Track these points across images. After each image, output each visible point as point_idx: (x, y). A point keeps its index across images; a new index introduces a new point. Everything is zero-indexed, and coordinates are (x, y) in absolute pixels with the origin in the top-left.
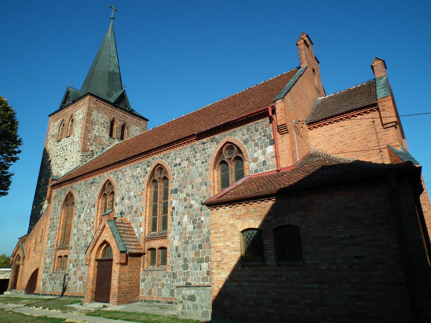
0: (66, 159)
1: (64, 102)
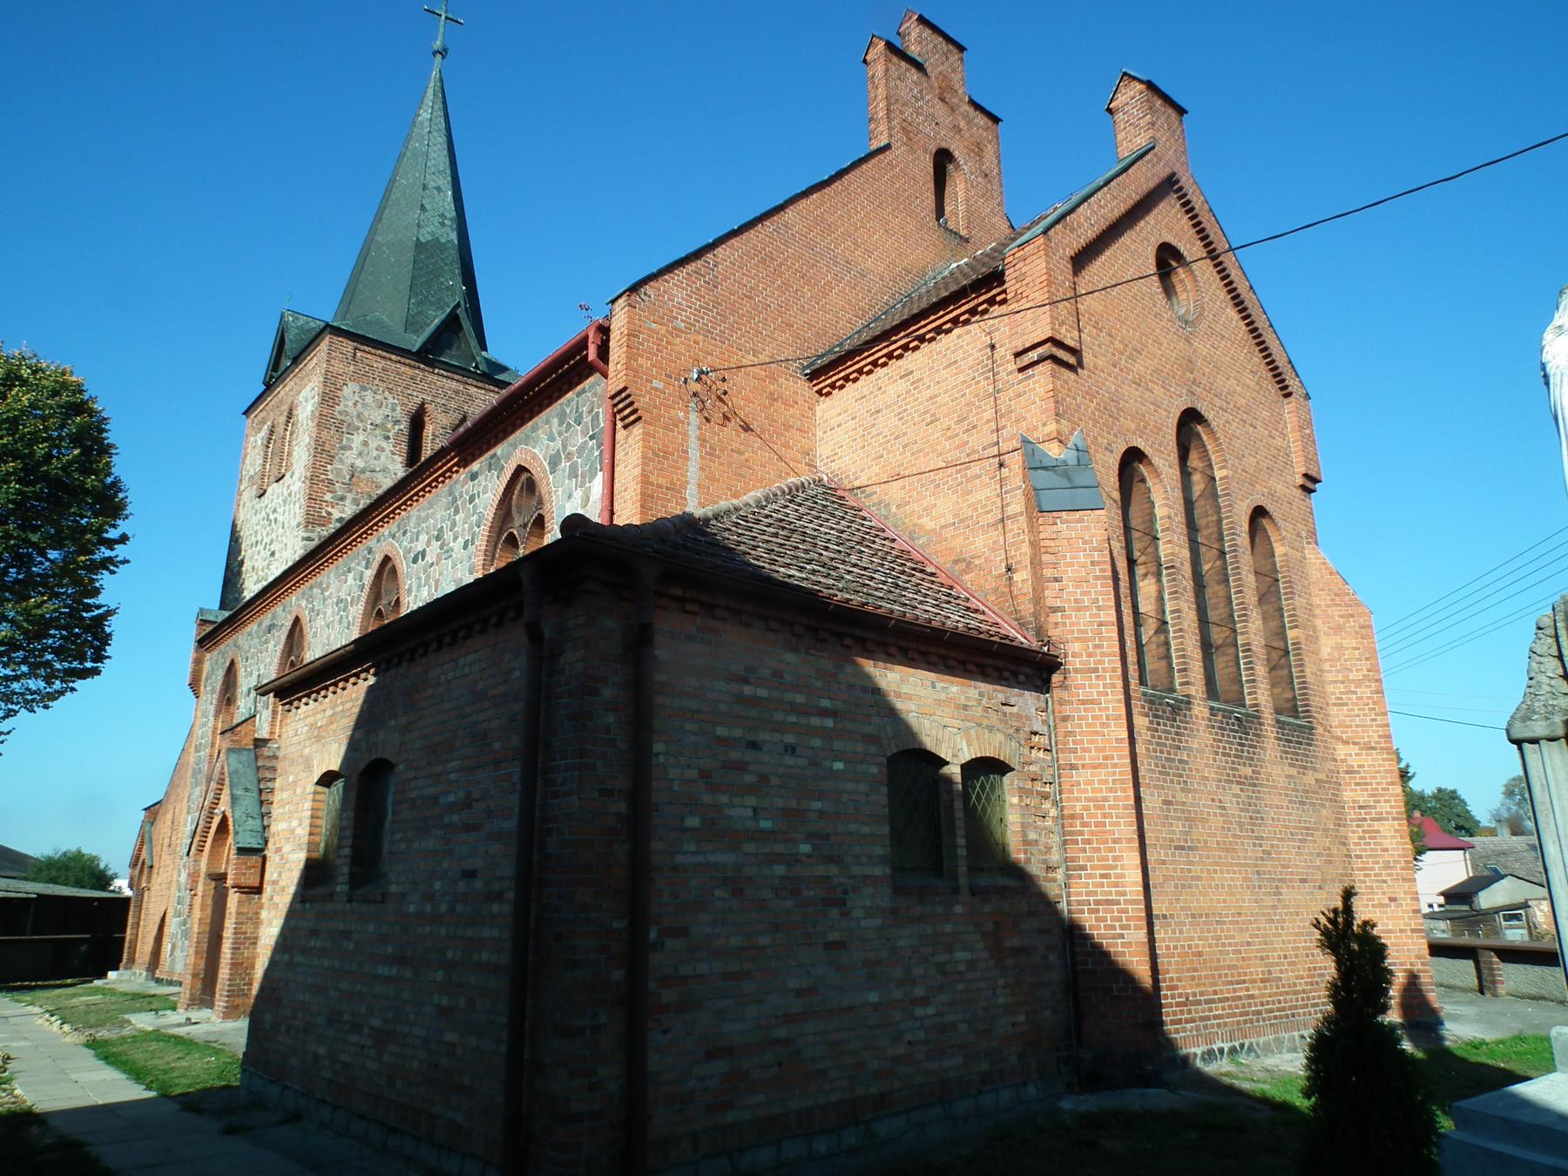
1: (275, 364)
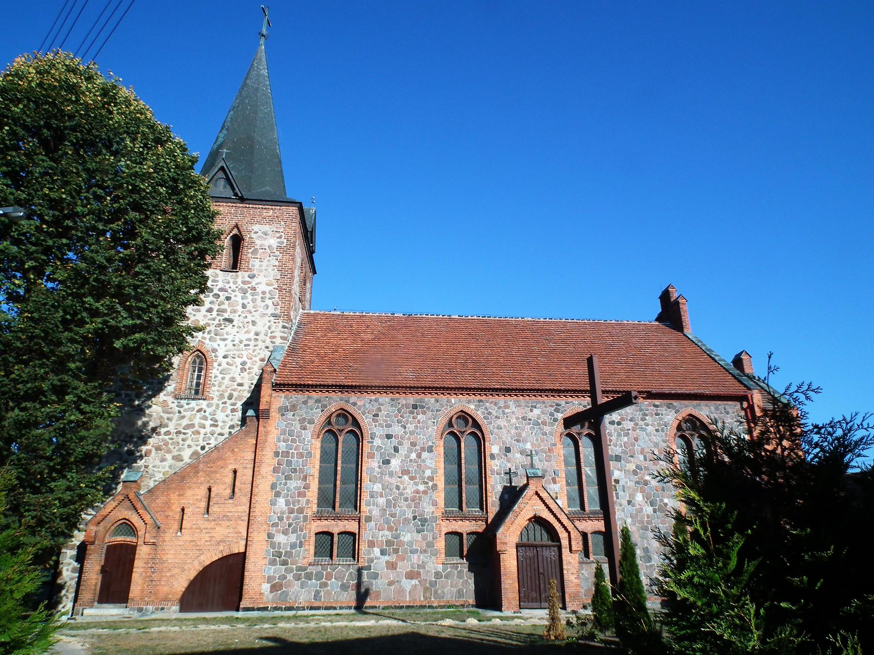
0: (230, 321)
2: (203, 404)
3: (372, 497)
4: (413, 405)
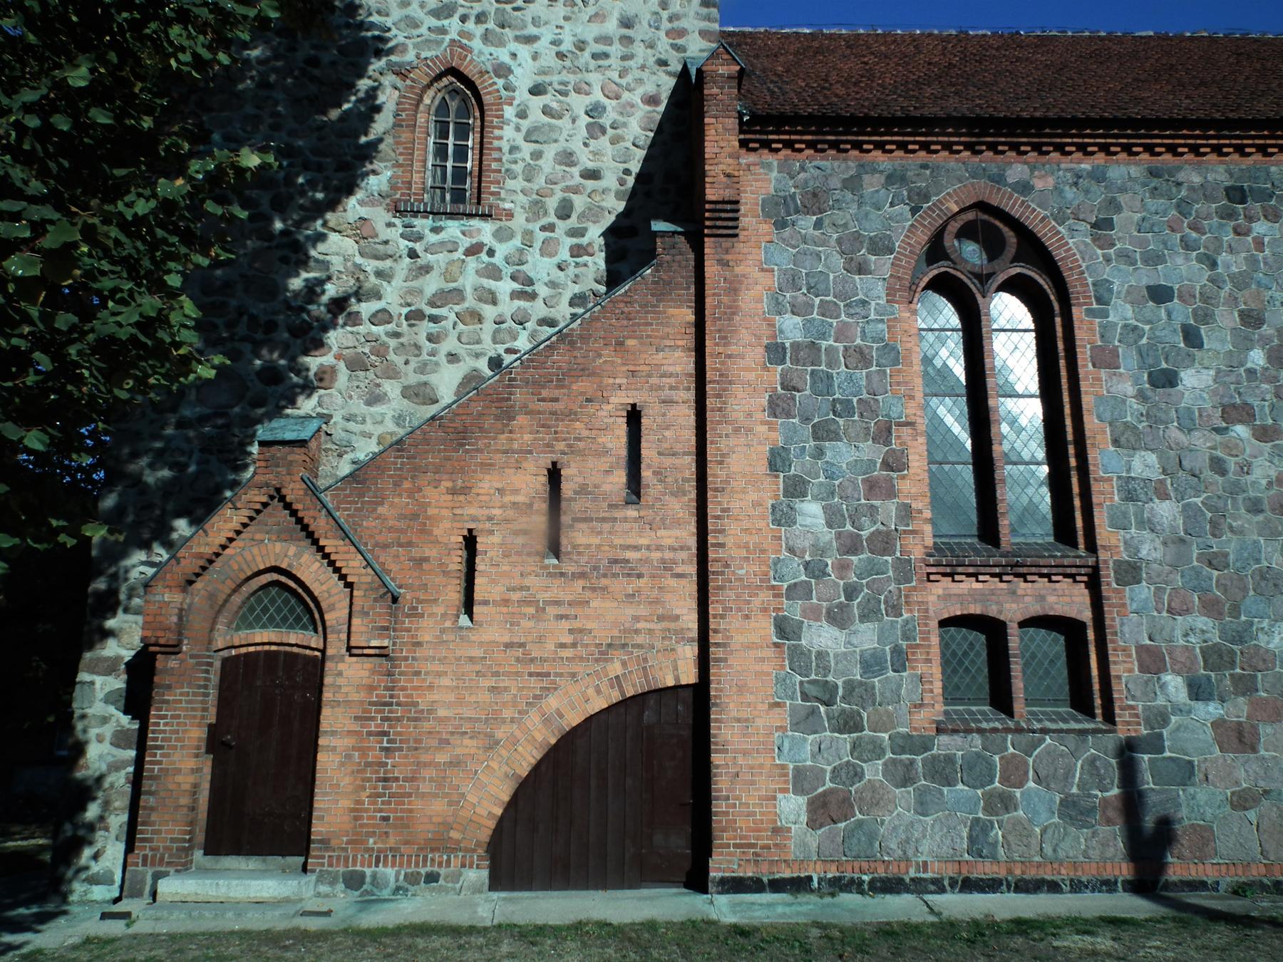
2: (485, 231)
3: (1130, 496)
4: (1227, 189)
